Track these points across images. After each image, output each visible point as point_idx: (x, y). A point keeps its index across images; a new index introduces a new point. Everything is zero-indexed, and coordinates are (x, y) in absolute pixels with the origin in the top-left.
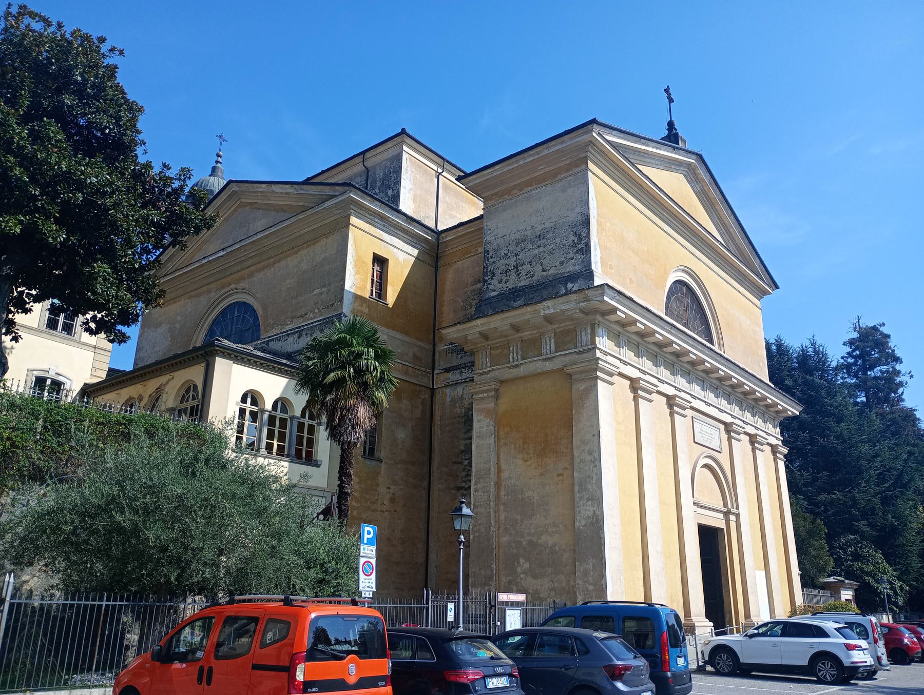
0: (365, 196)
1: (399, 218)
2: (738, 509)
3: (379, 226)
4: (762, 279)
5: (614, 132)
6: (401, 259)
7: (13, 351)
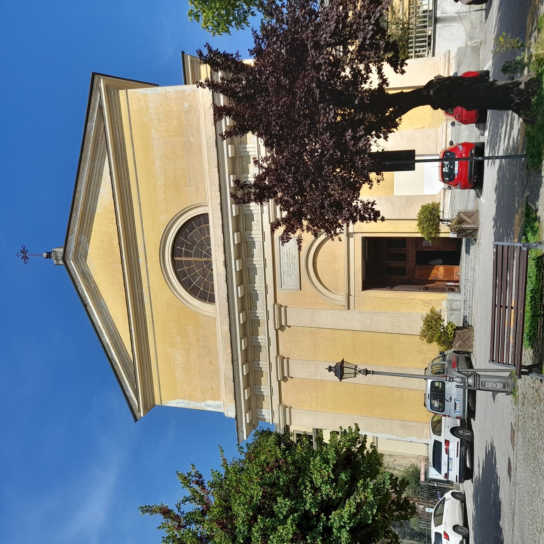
5: (128, 395)
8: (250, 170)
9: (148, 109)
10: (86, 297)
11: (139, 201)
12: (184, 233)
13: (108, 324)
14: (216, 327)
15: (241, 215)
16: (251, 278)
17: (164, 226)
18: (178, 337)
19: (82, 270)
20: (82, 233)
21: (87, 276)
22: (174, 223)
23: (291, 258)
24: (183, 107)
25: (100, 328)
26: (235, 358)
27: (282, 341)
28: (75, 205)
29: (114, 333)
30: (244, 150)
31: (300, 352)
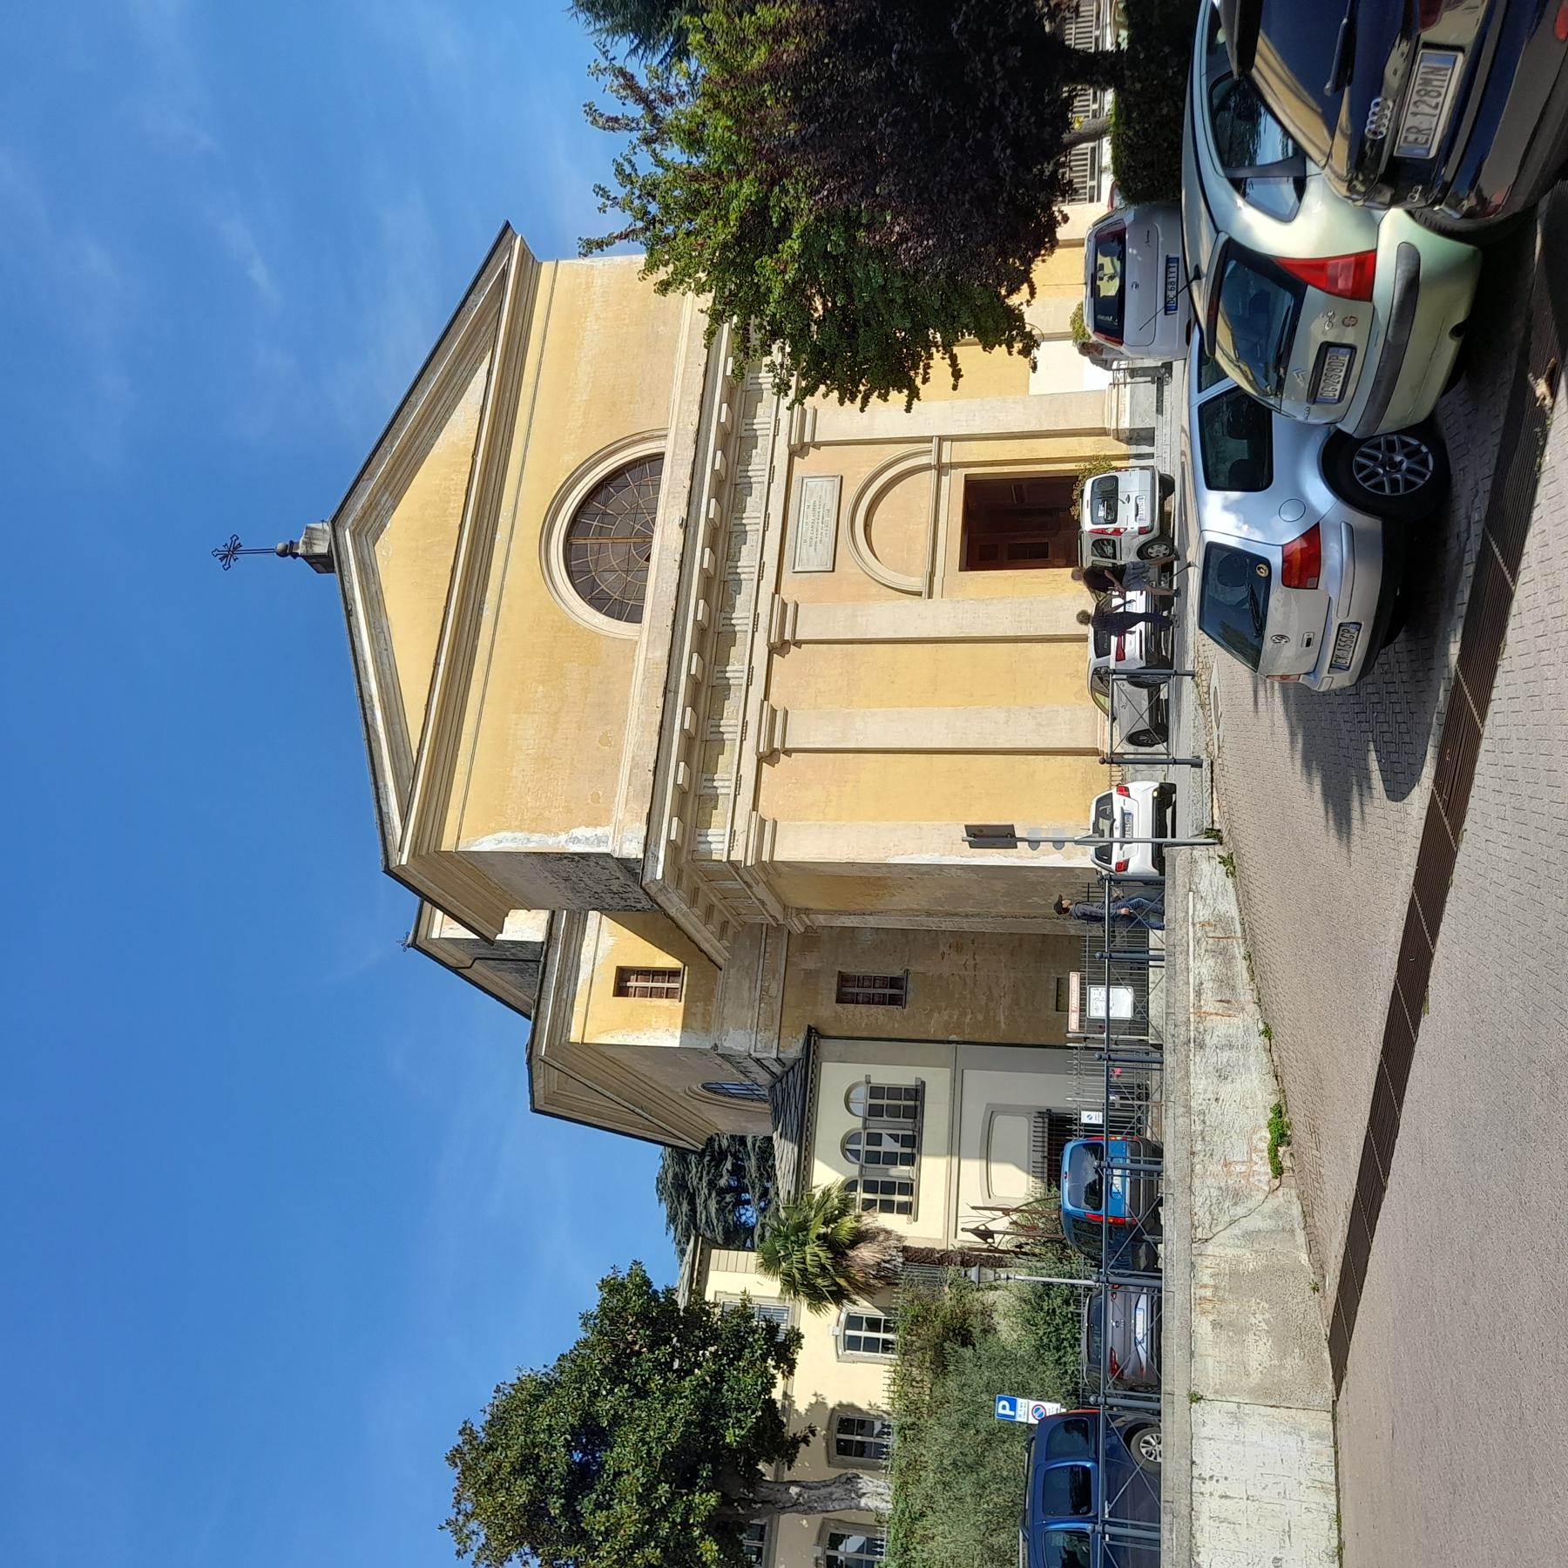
0: (538, 1030)
1: (554, 960)
2: (929, 440)
3: (571, 987)
4: (504, 274)
5: (384, 809)
6: (611, 941)
7: (819, 1393)
9: (589, 286)
11: (529, 430)
12: (604, 493)
14: (634, 661)
15: (729, 482)
17: (567, 471)
18: (540, 688)
21: (368, 570)
22: (597, 463)
25: (364, 662)
26: (672, 686)
27: (778, 678)
28: (396, 426)
31: (816, 696)
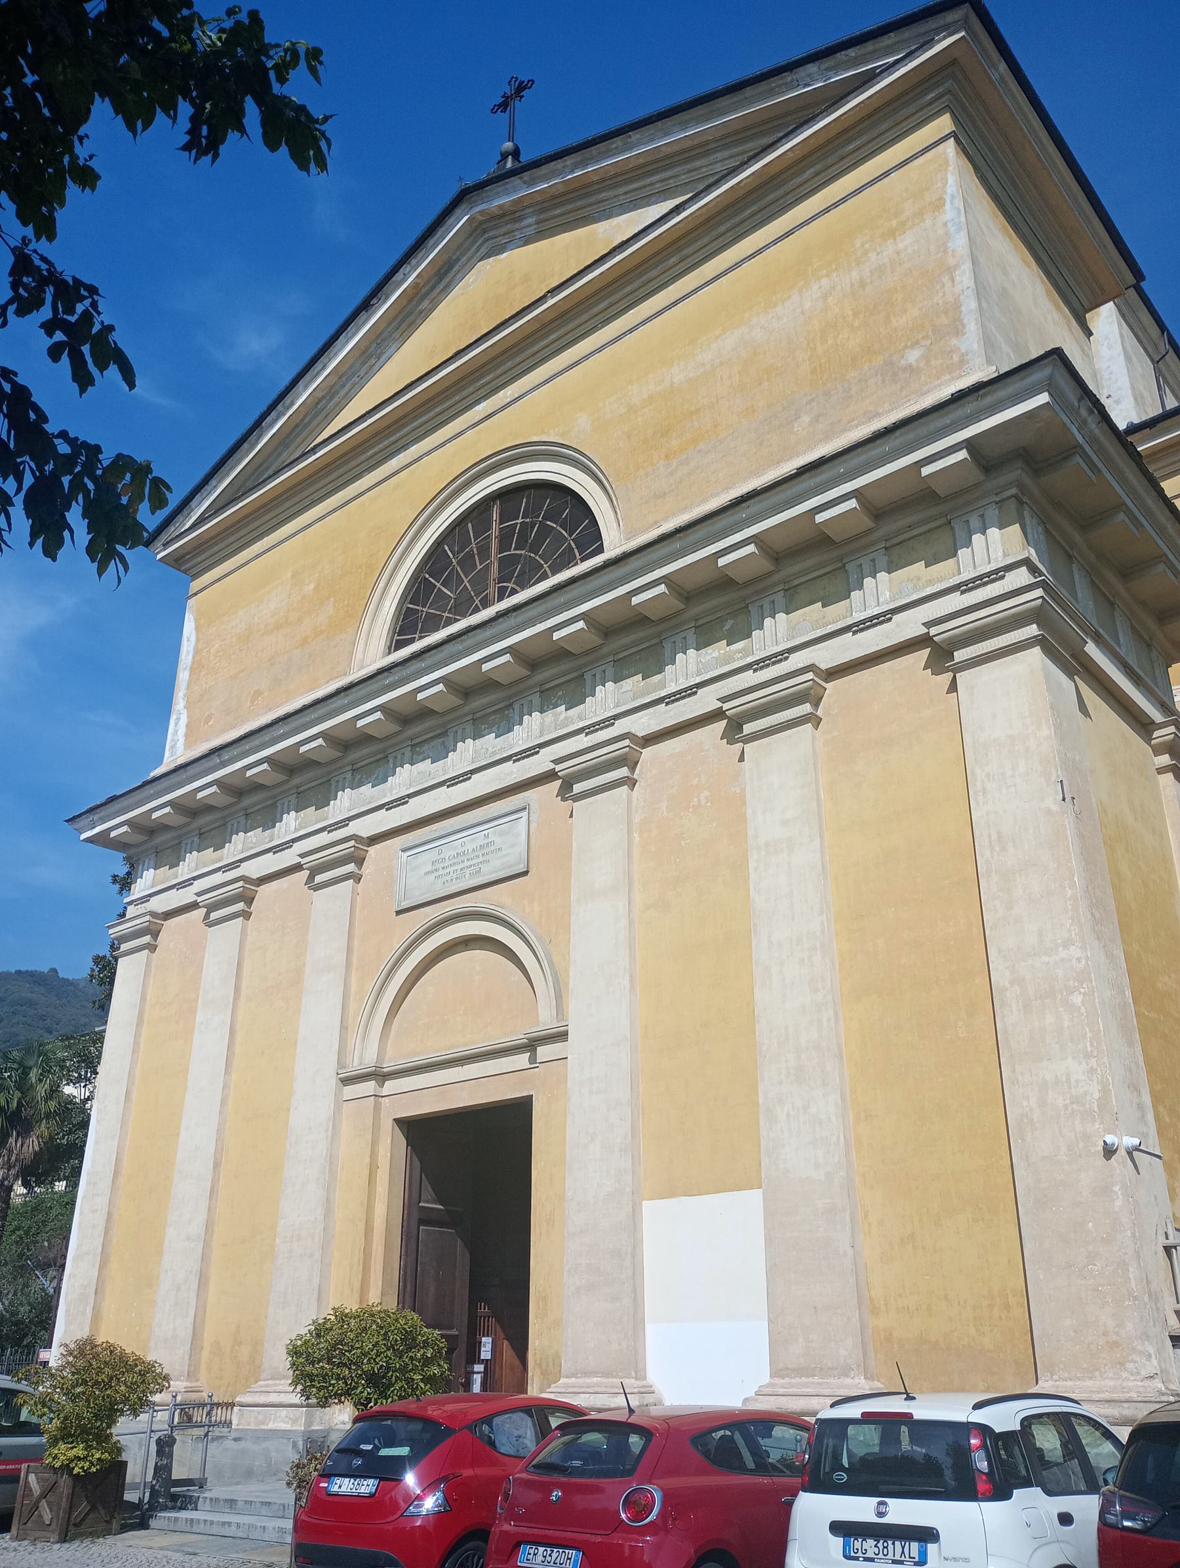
5: (194, 503)
8: (709, 649)
10: (387, 297)
13: (343, 386)
16: (426, 747)
19: (458, 260)
20: (542, 211)
23: (475, 861)
24: (906, 347)
25: (324, 367)
29: (324, 413)
30: (767, 607)
